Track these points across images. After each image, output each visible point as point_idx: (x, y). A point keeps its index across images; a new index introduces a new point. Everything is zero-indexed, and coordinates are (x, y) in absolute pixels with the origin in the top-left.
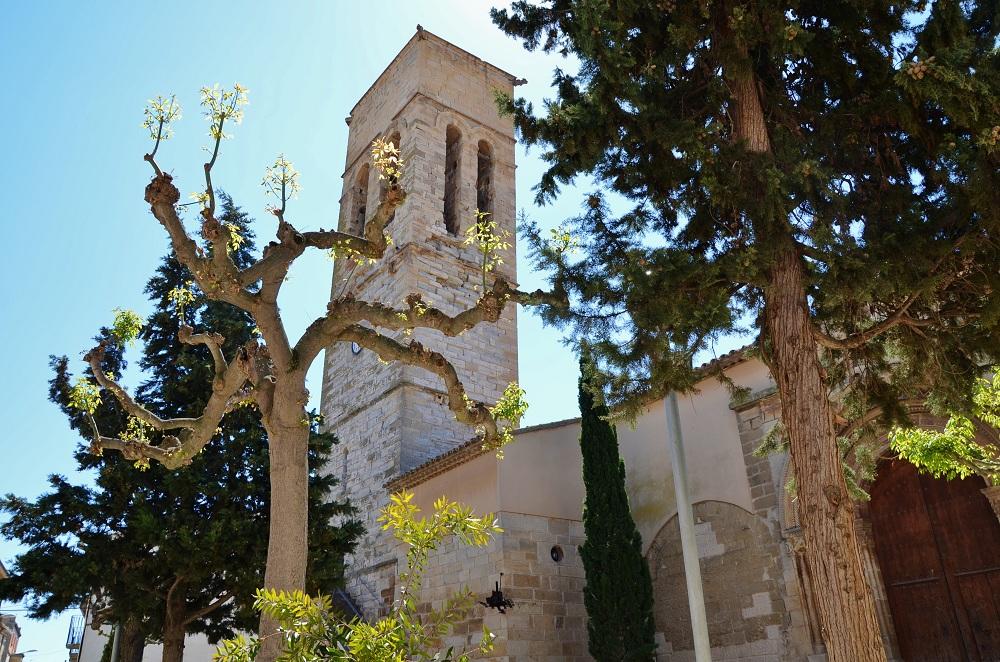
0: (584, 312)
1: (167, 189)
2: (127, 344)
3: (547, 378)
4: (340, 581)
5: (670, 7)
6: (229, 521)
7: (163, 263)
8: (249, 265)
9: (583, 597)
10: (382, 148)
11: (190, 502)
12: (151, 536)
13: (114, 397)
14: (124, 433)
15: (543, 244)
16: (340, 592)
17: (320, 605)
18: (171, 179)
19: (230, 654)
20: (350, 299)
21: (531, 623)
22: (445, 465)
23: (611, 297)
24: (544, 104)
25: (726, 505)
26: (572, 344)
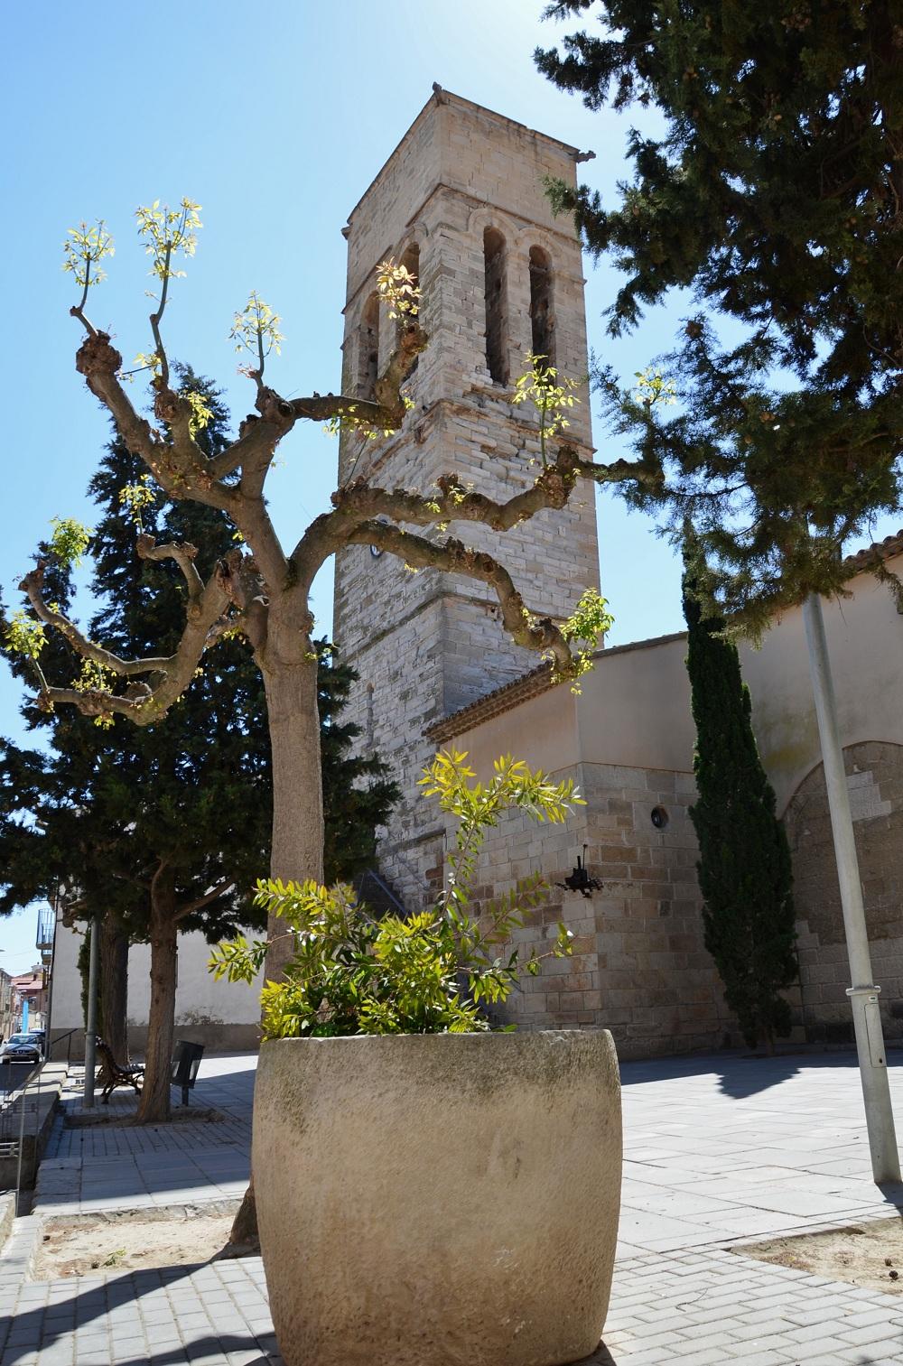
0: (684, 490)
1: (104, 354)
2: (73, 564)
3: (638, 581)
4: (372, 861)
5: (802, 22)
6: (222, 788)
7: (108, 453)
8: (222, 449)
9: (696, 875)
10: (391, 274)
11: (170, 764)
12: (125, 810)
13: (61, 634)
14: (78, 680)
15: (622, 397)
16: (371, 873)
17: (344, 894)
18: (108, 338)
19: (228, 960)
20: (361, 487)
21: (626, 910)
22: (503, 703)
23: (722, 466)
24: (618, 189)
25: (892, 747)
26: (668, 535)
